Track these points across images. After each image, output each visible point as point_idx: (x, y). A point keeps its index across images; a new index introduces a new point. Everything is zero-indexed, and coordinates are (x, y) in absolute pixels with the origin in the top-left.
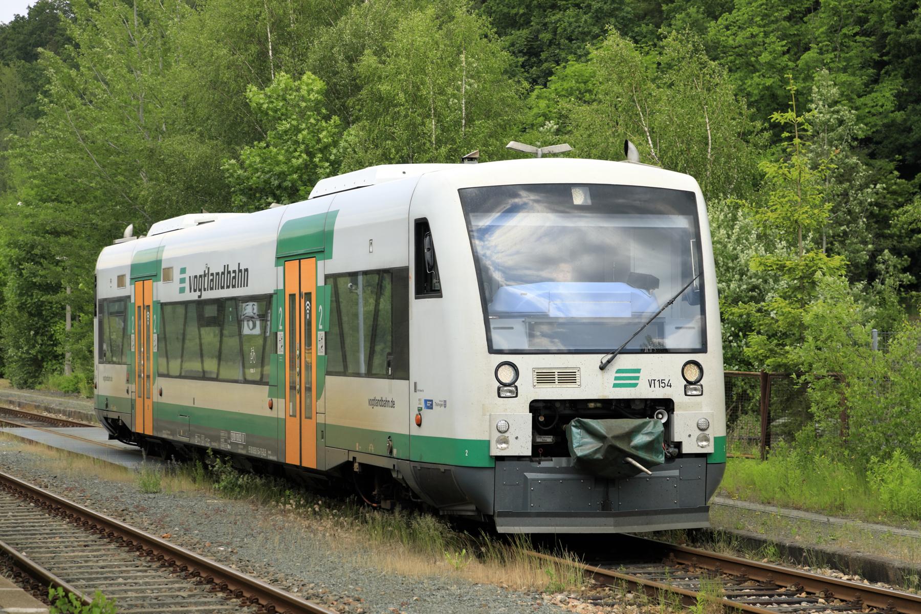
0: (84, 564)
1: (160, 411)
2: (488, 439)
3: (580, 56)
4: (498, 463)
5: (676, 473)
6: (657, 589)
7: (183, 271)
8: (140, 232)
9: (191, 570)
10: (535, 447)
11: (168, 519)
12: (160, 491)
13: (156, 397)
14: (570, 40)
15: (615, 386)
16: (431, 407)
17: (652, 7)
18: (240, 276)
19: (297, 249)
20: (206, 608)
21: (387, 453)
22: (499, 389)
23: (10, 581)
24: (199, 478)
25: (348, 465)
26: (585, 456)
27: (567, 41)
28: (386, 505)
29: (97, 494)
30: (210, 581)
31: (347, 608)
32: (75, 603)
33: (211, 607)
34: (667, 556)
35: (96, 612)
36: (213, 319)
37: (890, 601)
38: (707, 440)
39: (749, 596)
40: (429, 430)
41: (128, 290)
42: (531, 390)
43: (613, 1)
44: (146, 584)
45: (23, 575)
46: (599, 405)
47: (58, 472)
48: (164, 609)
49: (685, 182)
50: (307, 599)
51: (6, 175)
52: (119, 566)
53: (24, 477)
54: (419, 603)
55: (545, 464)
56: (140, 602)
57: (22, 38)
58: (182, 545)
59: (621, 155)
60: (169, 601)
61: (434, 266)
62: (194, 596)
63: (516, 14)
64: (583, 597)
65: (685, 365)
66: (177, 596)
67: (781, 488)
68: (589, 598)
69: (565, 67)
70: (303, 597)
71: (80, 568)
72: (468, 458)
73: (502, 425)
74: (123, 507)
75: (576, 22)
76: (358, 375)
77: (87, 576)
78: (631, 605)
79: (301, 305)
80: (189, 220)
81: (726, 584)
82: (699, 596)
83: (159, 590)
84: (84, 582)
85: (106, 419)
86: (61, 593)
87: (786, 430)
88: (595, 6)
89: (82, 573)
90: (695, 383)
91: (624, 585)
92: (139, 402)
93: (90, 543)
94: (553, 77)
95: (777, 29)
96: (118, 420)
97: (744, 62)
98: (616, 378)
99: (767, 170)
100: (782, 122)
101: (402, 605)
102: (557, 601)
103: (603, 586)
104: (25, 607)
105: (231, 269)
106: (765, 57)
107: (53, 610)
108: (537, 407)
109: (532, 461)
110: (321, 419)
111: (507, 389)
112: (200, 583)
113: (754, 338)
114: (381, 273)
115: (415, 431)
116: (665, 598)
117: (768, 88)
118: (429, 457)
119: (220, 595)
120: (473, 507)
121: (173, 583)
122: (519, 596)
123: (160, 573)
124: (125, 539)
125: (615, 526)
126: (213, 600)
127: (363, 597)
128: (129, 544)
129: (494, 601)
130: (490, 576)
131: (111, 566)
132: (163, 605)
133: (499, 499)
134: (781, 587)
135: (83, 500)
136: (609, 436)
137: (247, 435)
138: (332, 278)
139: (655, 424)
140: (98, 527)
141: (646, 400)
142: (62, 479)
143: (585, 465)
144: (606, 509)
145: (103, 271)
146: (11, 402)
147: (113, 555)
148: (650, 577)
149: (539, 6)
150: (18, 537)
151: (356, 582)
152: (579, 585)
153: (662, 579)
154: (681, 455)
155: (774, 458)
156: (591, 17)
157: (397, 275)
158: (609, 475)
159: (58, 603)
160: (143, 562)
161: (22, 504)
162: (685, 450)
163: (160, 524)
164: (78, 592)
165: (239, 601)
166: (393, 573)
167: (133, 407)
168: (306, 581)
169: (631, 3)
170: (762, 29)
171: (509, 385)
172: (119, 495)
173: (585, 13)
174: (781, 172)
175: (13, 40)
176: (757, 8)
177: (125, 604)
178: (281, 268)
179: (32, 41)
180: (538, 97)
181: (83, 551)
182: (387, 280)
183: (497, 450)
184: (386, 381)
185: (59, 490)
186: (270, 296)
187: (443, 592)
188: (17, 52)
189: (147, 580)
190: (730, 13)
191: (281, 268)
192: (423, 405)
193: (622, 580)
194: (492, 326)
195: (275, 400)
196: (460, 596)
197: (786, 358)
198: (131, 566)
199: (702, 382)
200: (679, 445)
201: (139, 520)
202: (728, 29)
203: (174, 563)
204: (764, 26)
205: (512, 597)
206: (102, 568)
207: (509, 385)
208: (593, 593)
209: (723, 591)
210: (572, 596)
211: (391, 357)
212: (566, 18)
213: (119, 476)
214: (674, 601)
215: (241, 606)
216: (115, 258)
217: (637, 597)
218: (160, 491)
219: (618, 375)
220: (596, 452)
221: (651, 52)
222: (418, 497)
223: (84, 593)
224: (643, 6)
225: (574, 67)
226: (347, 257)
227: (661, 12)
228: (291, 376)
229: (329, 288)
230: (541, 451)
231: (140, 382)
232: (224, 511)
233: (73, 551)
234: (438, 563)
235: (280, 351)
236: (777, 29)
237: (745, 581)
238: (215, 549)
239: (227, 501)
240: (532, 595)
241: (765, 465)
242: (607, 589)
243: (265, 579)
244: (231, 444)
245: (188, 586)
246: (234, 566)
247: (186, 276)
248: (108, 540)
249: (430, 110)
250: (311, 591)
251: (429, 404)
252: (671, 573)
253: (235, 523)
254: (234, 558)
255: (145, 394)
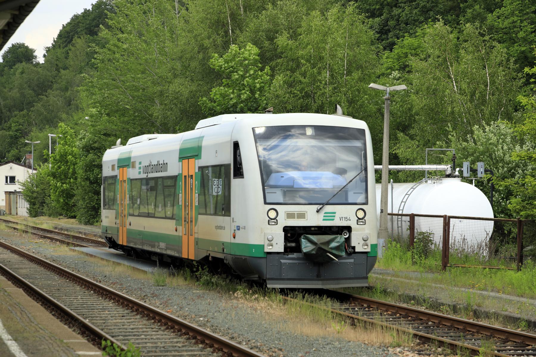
0: (122, 327)
1: (129, 232)
2: (263, 244)
3: (412, 34)
4: (269, 255)
5: (352, 261)
6: (456, 346)
7: (140, 163)
8: (124, 143)
9: (184, 331)
10: (286, 248)
11: (171, 301)
12: (166, 285)
13: (128, 227)
14: (407, 24)
15: (324, 220)
16: (239, 229)
17: (455, 4)
18: (163, 166)
19: (189, 154)
20: (192, 353)
21: (221, 251)
22: (269, 221)
23: (79, 336)
24: (188, 278)
25: (207, 257)
26: (308, 252)
27: (404, 25)
28: (224, 276)
29: (130, 286)
30: (195, 338)
31: (274, 354)
32: (117, 349)
33: (195, 353)
34: (349, 300)
35: (129, 355)
36: (159, 187)
37: (417, 314)
38: (367, 245)
39: (510, 350)
40: (238, 240)
41: (116, 172)
42: (284, 222)
43: (433, 2)
44: (158, 339)
45: (87, 333)
46: (316, 229)
47: (107, 274)
48: (168, 354)
49: (361, 124)
50: (251, 349)
51: (78, 101)
52: (142, 328)
53: (87, 276)
54: (316, 352)
55: (290, 256)
56: (154, 349)
57: (88, 22)
58: (178, 317)
59: (334, 111)
60: (171, 349)
61: (241, 164)
62: (185, 346)
63: (374, 9)
64: (412, 350)
65: (357, 210)
66: (176, 346)
67: (529, 288)
68: (416, 351)
69: (403, 40)
70: (248, 347)
71: (119, 329)
72: (254, 253)
73: (270, 237)
74: (144, 294)
75: (410, 14)
76: (211, 215)
77: (123, 334)
78: (440, 355)
79: (189, 180)
80: (145, 137)
81: (496, 343)
82: (481, 350)
83: (165, 342)
84: (121, 337)
85: (106, 237)
86: (109, 343)
87: (532, 253)
88: (422, 4)
89: (121, 332)
90: (362, 219)
91: (437, 343)
92: (121, 228)
93: (125, 315)
94: (396, 46)
95: (528, 19)
96: (111, 238)
97: (508, 37)
98: (324, 216)
99: (522, 101)
100: (531, 73)
101: (306, 353)
102: (397, 352)
103: (424, 343)
104: (88, 351)
105: (160, 163)
106: (521, 34)
107: (105, 353)
108: (286, 229)
109: (284, 254)
110: (196, 236)
111: (273, 221)
112: (189, 339)
113: (513, 200)
114: (220, 166)
115: (233, 241)
116: (461, 351)
117: (523, 52)
118: (238, 252)
119: (201, 346)
120: (257, 276)
121: (173, 338)
122: (375, 349)
123: (166, 333)
124: (146, 313)
125: (322, 285)
126: (197, 348)
127: (283, 348)
128: (148, 315)
129: (360, 351)
130: (358, 337)
131: (138, 328)
132: (167, 351)
133: (268, 271)
134: (529, 345)
135: (121, 290)
136: (318, 243)
137: (167, 244)
138: (201, 168)
139: (341, 238)
140: (130, 305)
141: (339, 227)
142: (109, 277)
143: (307, 255)
144: (318, 277)
145: (107, 162)
146: (80, 233)
147: (139, 322)
148: (452, 338)
149: (388, 4)
150: (84, 311)
151: (279, 339)
152: (410, 343)
153: (459, 340)
154: (355, 252)
155: (524, 270)
156: (419, 11)
157: (227, 167)
158: (319, 261)
159: (107, 349)
160: (156, 326)
161: (86, 291)
162: (357, 250)
163: (166, 304)
164: (119, 343)
165: (211, 350)
166: (301, 334)
167: (118, 231)
168: (250, 338)
169: (443, 2)
170: (519, 18)
171: (274, 219)
172: (142, 287)
173: (416, 8)
174: (530, 102)
175: (83, 24)
176: (516, 6)
177: (145, 351)
178: (181, 163)
179: (94, 24)
180: (387, 58)
181: (121, 319)
182: (220, 170)
183: (268, 249)
184: (222, 217)
185: (107, 284)
186: (177, 176)
187: (330, 346)
188: (85, 31)
189: (158, 337)
190: (500, 9)
191: (181, 163)
192: (236, 229)
193: (435, 340)
194: (266, 192)
195: (178, 227)
196: (340, 348)
197: (533, 211)
198: (149, 328)
199: (365, 218)
200: (354, 248)
201: (154, 302)
202: (499, 18)
203: (174, 327)
204: (520, 17)
205: (371, 349)
206: (132, 329)
207: (274, 219)
208: (418, 347)
209: (495, 347)
210: (406, 349)
211: (224, 206)
212: (405, 11)
213: (141, 276)
214: (466, 353)
215: (213, 353)
216: (111, 155)
217: (444, 350)
218: (166, 285)
219: (325, 215)
220: (313, 250)
221: (454, 32)
222: (235, 272)
223: (122, 344)
224: (450, 3)
225: (408, 40)
226: (208, 159)
227: (460, 8)
228: (185, 215)
229: (200, 172)
230: (288, 250)
231: (185, 225)
232: (203, 297)
233: (116, 319)
234: (327, 329)
235: (180, 204)
236: (528, 19)
237: (508, 342)
238: (198, 319)
239: (205, 291)
240: (382, 348)
241: (520, 273)
242: (426, 345)
243: (227, 337)
244: (160, 249)
245: (182, 340)
246: (208, 329)
247: (141, 166)
248: (136, 313)
249: (326, 64)
250: (253, 344)
251: (238, 228)
252: (464, 336)
253: (209, 304)
254: (209, 324)
255: (123, 225)
